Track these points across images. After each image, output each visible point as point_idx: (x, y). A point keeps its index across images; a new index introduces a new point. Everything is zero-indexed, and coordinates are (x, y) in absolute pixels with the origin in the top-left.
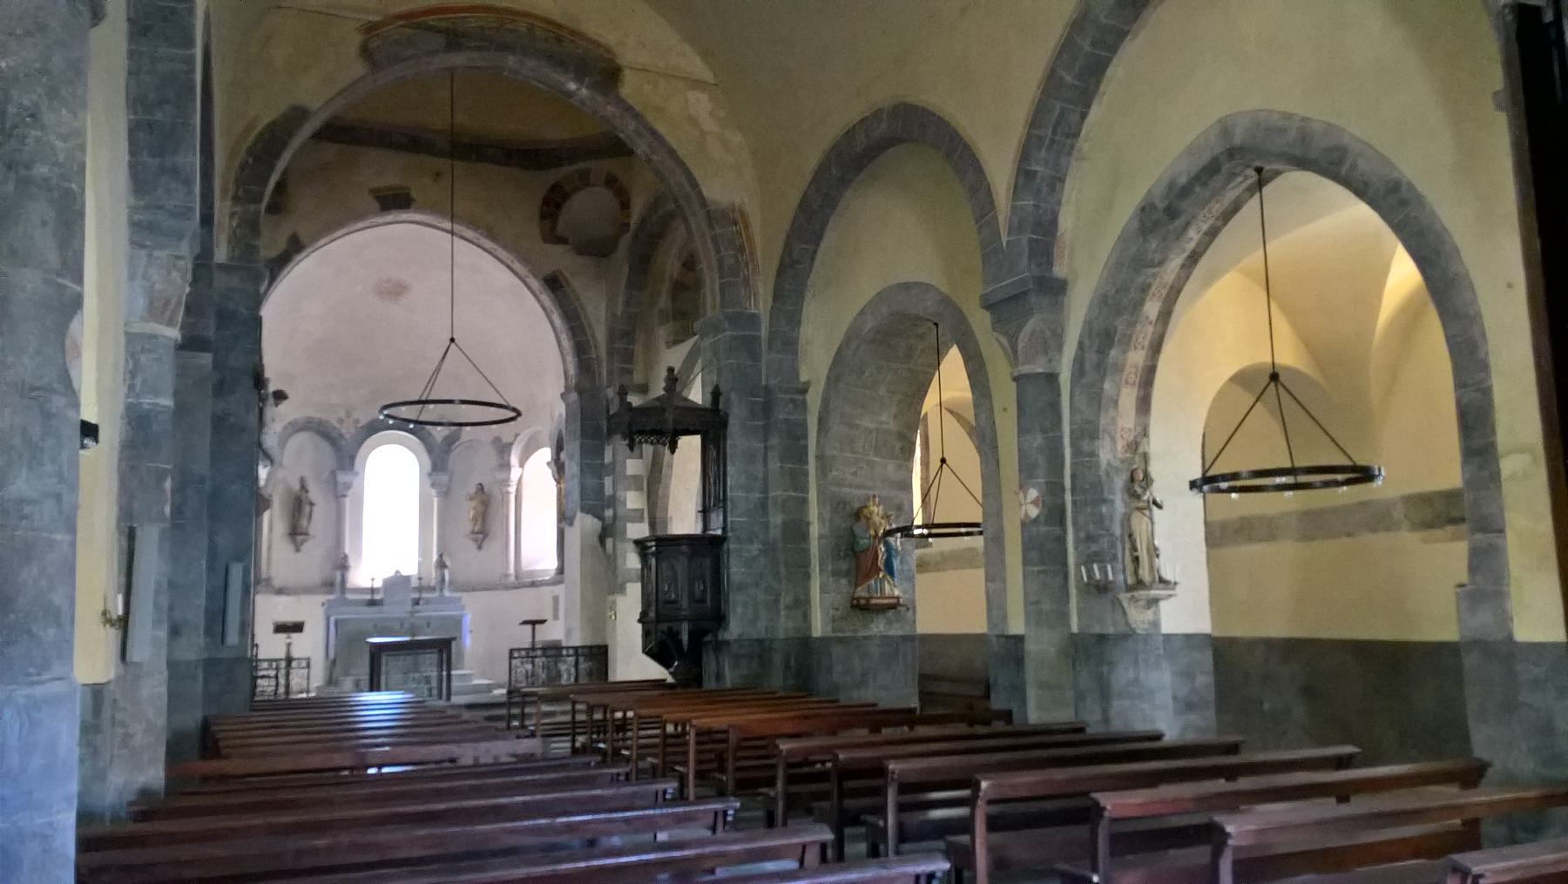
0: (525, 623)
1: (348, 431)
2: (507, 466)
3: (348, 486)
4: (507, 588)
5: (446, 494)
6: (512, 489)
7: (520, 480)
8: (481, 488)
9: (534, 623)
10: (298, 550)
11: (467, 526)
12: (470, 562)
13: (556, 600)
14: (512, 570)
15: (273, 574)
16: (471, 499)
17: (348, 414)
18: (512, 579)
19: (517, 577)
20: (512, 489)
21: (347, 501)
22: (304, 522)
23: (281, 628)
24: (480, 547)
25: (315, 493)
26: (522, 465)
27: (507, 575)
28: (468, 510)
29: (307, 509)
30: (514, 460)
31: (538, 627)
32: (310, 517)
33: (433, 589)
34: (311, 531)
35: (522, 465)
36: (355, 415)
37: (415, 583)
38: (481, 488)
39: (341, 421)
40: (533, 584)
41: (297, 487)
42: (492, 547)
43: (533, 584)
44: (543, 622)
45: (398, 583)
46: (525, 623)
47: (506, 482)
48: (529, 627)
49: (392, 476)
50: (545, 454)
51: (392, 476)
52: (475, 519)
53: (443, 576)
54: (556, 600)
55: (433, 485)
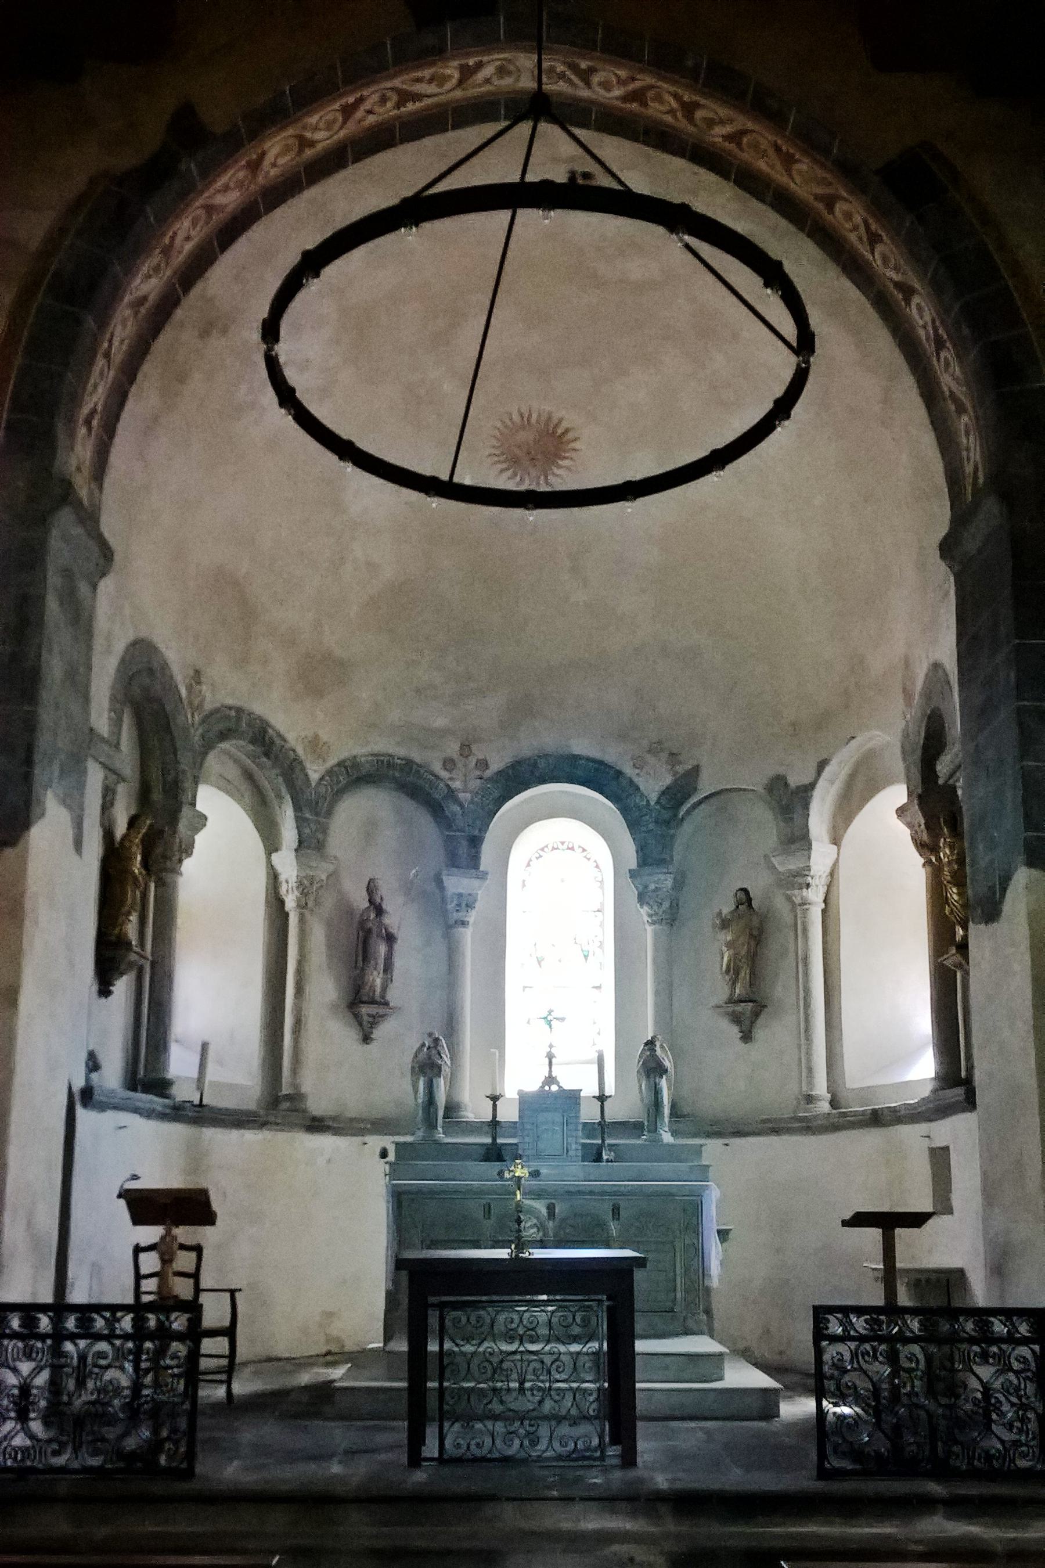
0: (860, 1220)
1: (464, 784)
2: (798, 840)
3: (467, 903)
4: (808, 1127)
5: (671, 917)
6: (815, 896)
7: (832, 873)
8: (745, 898)
9: (889, 1222)
10: (366, 1039)
11: (719, 990)
12: (729, 1070)
13: (940, 1158)
14: (821, 1087)
15: (307, 1086)
16: (725, 924)
17: (466, 748)
18: (824, 1107)
19: (834, 1103)
20: (815, 896)
21: (468, 937)
22: (376, 979)
23: (143, 1206)
24: (747, 1037)
25: (400, 916)
26: (836, 841)
27: (810, 1099)
28: (716, 951)
29: (382, 949)
30: (819, 819)
31: (902, 1234)
32: (388, 967)
33: (634, 1128)
34: (393, 996)
35: (836, 841)
36: (479, 752)
37: (589, 1113)
38: (745, 898)
39: (449, 764)
40: (876, 1119)
41: (360, 901)
42: (776, 1033)
43: (876, 1119)
44: (917, 1220)
45: (554, 1103)
46: (860, 1220)
47: (799, 879)
48: (874, 1234)
49: (559, 885)
50: (897, 794)
51: (559, 885)
52: (733, 972)
53: (668, 1103)
54: (940, 1158)
55: (642, 898)
